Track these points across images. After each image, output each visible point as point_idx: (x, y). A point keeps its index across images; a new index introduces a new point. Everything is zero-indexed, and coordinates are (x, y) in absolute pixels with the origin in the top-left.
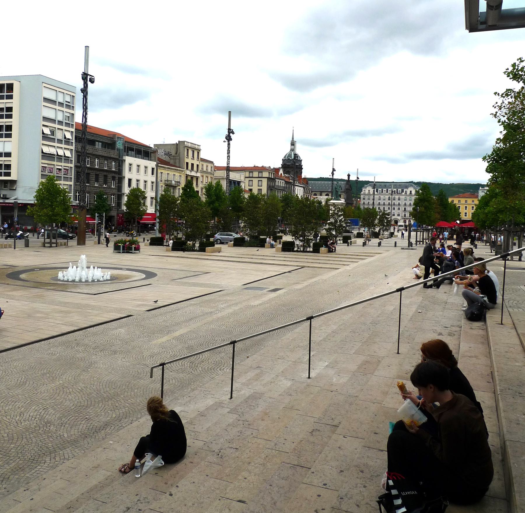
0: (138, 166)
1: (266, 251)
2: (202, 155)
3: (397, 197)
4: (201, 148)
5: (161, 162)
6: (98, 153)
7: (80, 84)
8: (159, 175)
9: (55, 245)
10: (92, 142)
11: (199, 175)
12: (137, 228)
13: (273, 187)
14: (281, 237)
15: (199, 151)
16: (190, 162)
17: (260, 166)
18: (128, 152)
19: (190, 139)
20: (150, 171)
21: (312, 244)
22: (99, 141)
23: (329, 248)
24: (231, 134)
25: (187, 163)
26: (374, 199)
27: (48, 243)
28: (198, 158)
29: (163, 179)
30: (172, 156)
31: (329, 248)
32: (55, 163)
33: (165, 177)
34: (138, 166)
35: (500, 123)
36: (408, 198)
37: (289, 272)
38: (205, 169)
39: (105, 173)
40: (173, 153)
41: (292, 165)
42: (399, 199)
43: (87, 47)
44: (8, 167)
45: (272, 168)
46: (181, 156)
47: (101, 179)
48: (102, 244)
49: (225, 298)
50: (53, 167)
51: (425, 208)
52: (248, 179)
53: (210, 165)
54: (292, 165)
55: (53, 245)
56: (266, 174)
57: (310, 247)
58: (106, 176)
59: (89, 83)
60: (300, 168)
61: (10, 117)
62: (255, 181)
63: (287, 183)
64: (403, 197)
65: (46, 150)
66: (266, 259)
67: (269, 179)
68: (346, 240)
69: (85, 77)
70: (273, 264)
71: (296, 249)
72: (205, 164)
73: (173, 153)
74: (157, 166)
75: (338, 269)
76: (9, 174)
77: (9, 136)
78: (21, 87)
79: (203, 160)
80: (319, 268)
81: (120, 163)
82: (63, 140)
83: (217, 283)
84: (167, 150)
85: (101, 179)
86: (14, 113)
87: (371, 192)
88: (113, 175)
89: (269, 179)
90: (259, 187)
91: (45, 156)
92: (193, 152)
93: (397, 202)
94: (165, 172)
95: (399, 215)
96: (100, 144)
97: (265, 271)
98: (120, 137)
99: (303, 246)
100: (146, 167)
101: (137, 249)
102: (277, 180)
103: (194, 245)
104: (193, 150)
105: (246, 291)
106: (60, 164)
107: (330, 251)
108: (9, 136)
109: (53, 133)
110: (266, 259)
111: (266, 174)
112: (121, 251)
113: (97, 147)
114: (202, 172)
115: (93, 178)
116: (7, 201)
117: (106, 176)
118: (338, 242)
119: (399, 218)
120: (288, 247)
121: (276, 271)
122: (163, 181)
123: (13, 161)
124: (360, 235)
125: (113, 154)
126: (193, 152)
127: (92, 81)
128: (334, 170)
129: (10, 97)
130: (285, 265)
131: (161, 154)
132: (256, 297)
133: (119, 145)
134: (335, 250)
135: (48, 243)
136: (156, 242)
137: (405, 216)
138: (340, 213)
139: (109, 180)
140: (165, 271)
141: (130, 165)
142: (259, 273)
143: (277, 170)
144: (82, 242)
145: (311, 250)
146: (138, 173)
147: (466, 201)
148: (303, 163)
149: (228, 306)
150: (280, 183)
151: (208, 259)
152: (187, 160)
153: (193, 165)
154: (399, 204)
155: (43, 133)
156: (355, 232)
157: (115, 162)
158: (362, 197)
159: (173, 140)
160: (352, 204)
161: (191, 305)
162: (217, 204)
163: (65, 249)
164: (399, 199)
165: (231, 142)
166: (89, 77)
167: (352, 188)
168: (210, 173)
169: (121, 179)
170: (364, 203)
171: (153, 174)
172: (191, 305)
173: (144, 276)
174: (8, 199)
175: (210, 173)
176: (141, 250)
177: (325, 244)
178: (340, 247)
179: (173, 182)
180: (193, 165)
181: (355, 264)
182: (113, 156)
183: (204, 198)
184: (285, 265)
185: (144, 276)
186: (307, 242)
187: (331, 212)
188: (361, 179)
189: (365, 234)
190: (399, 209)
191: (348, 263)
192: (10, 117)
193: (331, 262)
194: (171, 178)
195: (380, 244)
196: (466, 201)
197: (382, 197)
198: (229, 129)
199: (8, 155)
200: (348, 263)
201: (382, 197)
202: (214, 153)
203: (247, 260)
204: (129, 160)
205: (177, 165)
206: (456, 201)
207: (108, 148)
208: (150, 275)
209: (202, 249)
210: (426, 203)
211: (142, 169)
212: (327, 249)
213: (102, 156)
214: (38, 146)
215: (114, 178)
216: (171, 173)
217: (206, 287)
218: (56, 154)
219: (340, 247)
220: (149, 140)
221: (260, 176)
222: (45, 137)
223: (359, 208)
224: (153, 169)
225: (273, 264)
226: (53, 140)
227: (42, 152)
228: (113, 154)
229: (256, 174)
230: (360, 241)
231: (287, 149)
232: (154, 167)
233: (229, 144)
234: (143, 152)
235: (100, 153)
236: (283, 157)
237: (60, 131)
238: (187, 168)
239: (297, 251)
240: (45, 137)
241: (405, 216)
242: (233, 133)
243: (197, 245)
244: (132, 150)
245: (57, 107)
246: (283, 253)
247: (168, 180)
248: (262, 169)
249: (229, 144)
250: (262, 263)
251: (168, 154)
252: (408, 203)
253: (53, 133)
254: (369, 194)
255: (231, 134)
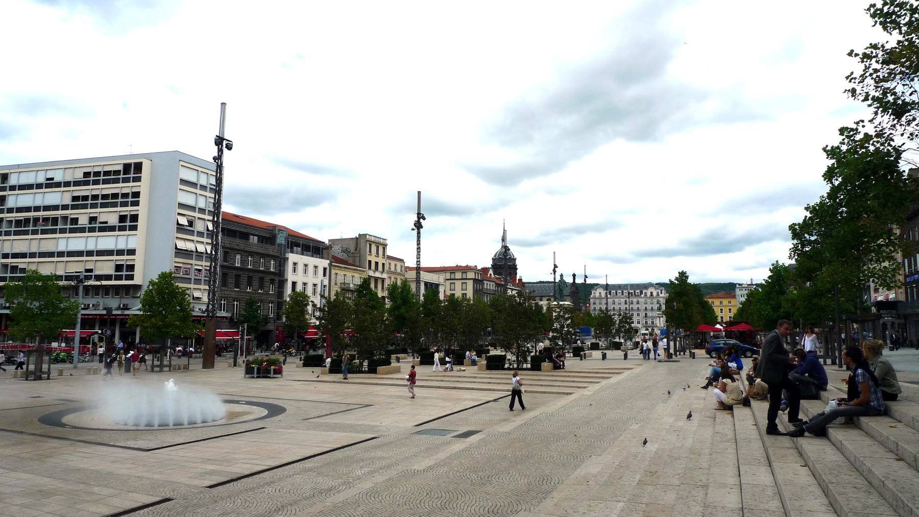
0: (306, 265)
1: (470, 370)
2: (389, 252)
3: (635, 300)
4: (388, 242)
5: (335, 260)
6: (251, 250)
7: (214, 151)
8: (333, 277)
9: (167, 369)
10: (245, 236)
11: (385, 276)
12: (296, 345)
13: (481, 290)
14: (488, 351)
15: (385, 246)
16: (373, 259)
17: (464, 265)
18: (292, 248)
19: (374, 230)
20: (321, 271)
21: (529, 359)
22: (254, 235)
23: (555, 363)
24: (421, 220)
25: (370, 262)
26: (607, 304)
27: (157, 366)
28: (384, 255)
29: (339, 282)
30: (353, 252)
31: (555, 363)
32: (193, 262)
33: (340, 279)
34: (306, 265)
35: (870, 102)
36: (649, 301)
37: (495, 400)
38: (393, 269)
39: (261, 275)
40: (352, 249)
41: (505, 264)
42: (638, 303)
43: (223, 104)
44: (131, 268)
45: (479, 268)
46: (362, 253)
47: (256, 283)
48: (240, 366)
49: (373, 455)
50: (189, 266)
51: (685, 304)
52: (448, 282)
53: (399, 264)
54: (505, 264)
55: (165, 369)
56: (471, 275)
57: (526, 361)
58: (261, 279)
59: (225, 150)
60: (514, 268)
61: (136, 204)
62: (458, 284)
63: (497, 285)
64: (643, 300)
65: (181, 245)
66: (462, 382)
67: (475, 280)
68: (578, 352)
69: (219, 141)
70: (472, 389)
71: (506, 366)
72: (393, 263)
73: (352, 249)
74: (330, 265)
75: (570, 394)
76: (131, 277)
77: (134, 228)
78: (152, 166)
79: (390, 258)
80: (541, 392)
81: (282, 262)
82: (206, 232)
83: (375, 424)
84: (345, 246)
85: (256, 283)
86: (142, 199)
87: (603, 295)
88: (272, 277)
89: (475, 280)
90: (465, 290)
91: (179, 252)
92: (378, 247)
93: (635, 306)
94: (341, 273)
95: (639, 323)
96: (256, 238)
97: (459, 399)
98: (282, 229)
99: (518, 362)
100: (316, 267)
101: (279, 371)
102: (485, 282)
103: (361, 364)
104: (378, 244)
105: (418, 437)
106: (200, 263)
107: (557, 367)
108: (134, 228)
109: (191, 223)
110: (462, 382)
111: (471, 275)
112: (255, 375)
113: (251, 241)
114: (389, 272)
115: (244, 280)
116: (126, 312)
117: (261, 279)
118: (567, 355)
119: (639, 326)
120: (496, 364)
121: (474, 400)
122: (339, 285)
123: (138, 260)
124: (595, 347)
125: (271, 250)
126: (378, 247)
127: (229, 147)
128: (555, 266)
129: (138, 179)
130: (489, 390)
131: (337, 250)
132: (430, 450)
133: (281, 239)
134: (564, 365)
135: (157, 366)
136: (312, 362)
137: (646, 323)
138: (567, 316)
139: (267, 284)
140: (301, 404)
141: (295, 264)
142: (448, 404)
143: (485, 270)
144: (208, 364)
145: (529, 366)
146: (305, 275)
147: (721, 302)
148: (517, 262)
149: (371, 473)
150: (489, 286)
151: (377, 384)
152: (369, 258)
153: (377, 263)
154: (638, 309)
155: (178, 224)
156: (588, 343)
157: (274, 260)
158: (592, 301)
159: (351, 233)
160: (580, 310)
161: (306, 470)
162: (403, 310)
163: (184, 374)
164: (638, 303)
165: (421, 230)
166: (225, 142)
167: (580, 292)
168: (400, 274)
169: (282, 283)
170: (595, 309)
171: (324, 275)
172: (306, 470)
173: (265, 412)
174: (128, 309)
175: (400, 274)
176: (284, 373)
177: (551, 359)
178: (570, 362)
179: (351, 285)
180: (377, 263)
181: (597, 386)
182: (271, 253)
183: (388, 304)
184: (489, 390)
185: (265, 412)
186: (522, 355)
187: (554, 314)
188: (589, 281)
189: (601, 344)
190: (638, 315)
191: (585, 385)
192: (136, 204)
193: (559, 384)
194: (348, 280)
195: (626, 357)
196: (721, 302)
197: (616, 300)
198: (419, 214)
199: (132, 252)
200: (585, 385)
201: (616, 300)
202: (402, 249)
203: (438, 384)
204: (292, 257)
205: (358, 263)
206: (710, 301)
207: (266, 243)
208: (275, 410)
209: (372, 370)
210: (684, 298)
211: (311, 269)
212: (551, 364)
213: (258, 254)
214: (170, 240)
215: (272, 281)
216: (349, 274)
217: (351, 431)
218: (194, 249)
219: (570, 362)
220: (324, 237)
221: (464, 277)
222: (180, 228)
223: (589, 314)
224: (325, 269)
225: (472, 389)
226: (191, 233)
227: (176, 248)
228: (271, 250)
229: (458, 275)
230: (597, 354)
231: (497, 247)
232: (327, 266)
233: (419, 233)
234: (313, 248)
235: (255, 249)
236: (493, 256)
237: (202, 222)
238: (370, 268)
239: (509, 369)
240: (180, 228)
241: (646, 323)
242: (424, 219)
243: (366, 363)
244: (298, 245)
245: (199, 191)
246: (488, 372)
247: (344, 283)
248: (465, 269)
249: (419, 233)
250: (455, 388)
251: (346, 251)
252: (649, 307)
253: (191, 223)
254: (600, 298)
255: (421, 220)
